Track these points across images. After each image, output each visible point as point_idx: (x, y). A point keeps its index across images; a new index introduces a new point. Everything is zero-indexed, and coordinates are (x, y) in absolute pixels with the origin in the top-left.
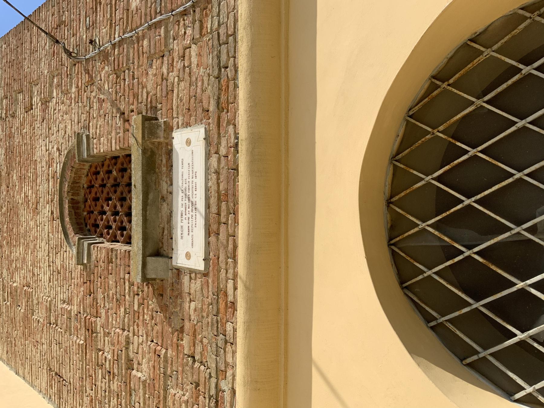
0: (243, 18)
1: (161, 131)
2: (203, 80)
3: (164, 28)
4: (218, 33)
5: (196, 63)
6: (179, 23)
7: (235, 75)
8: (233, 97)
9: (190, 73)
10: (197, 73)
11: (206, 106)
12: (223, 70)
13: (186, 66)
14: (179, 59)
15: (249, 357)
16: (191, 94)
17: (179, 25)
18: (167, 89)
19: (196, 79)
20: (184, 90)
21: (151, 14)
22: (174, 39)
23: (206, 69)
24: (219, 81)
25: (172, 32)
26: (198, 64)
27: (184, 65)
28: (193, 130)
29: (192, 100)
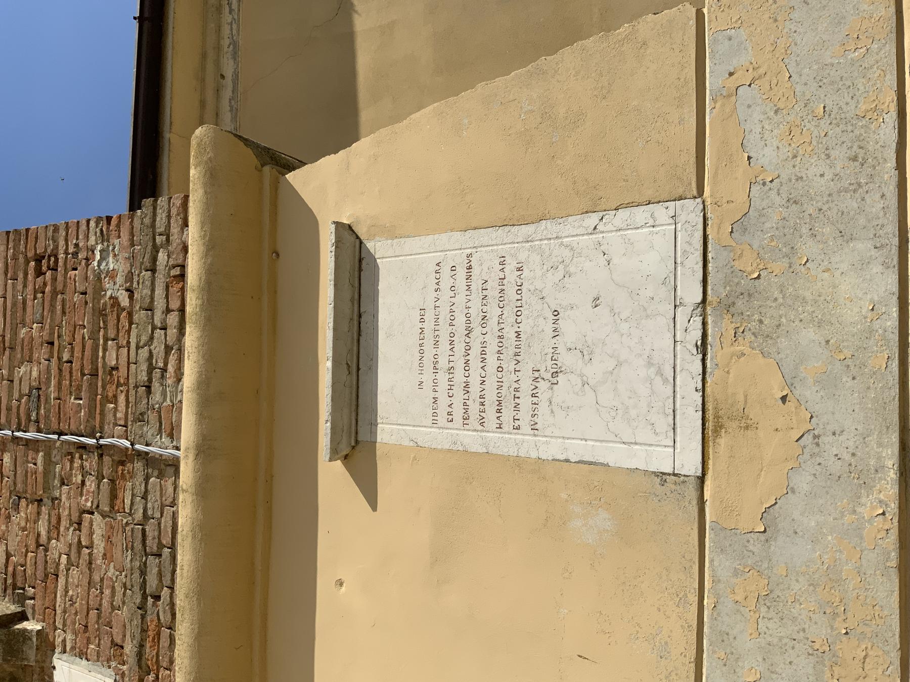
0: (185, 575)
1: (31, 648)
2: (113, 587)
3: (44, 457)
4: (144, 531)
5: (102, 550)
6: (72, 457)
7: (172, 622)
8: (167, 659)
9: (90, 563)
10: (103, 572)
11: (118, 640)
12: (150, 600)
13: (84, 544)
14: (71, 525)
15: (211, 220)
16: (91, 603)
17: (72, 462)
18: (46, 569)
19: (102, 580)
20: (77, 586)
21: (18, 414)
22: (63, 484)
23: (121, 572)
24: (143, 617)
25: (58, 468)
26: (105, 555)
27: (79, 542)
28: (92, 673)
29: (93, 614)
